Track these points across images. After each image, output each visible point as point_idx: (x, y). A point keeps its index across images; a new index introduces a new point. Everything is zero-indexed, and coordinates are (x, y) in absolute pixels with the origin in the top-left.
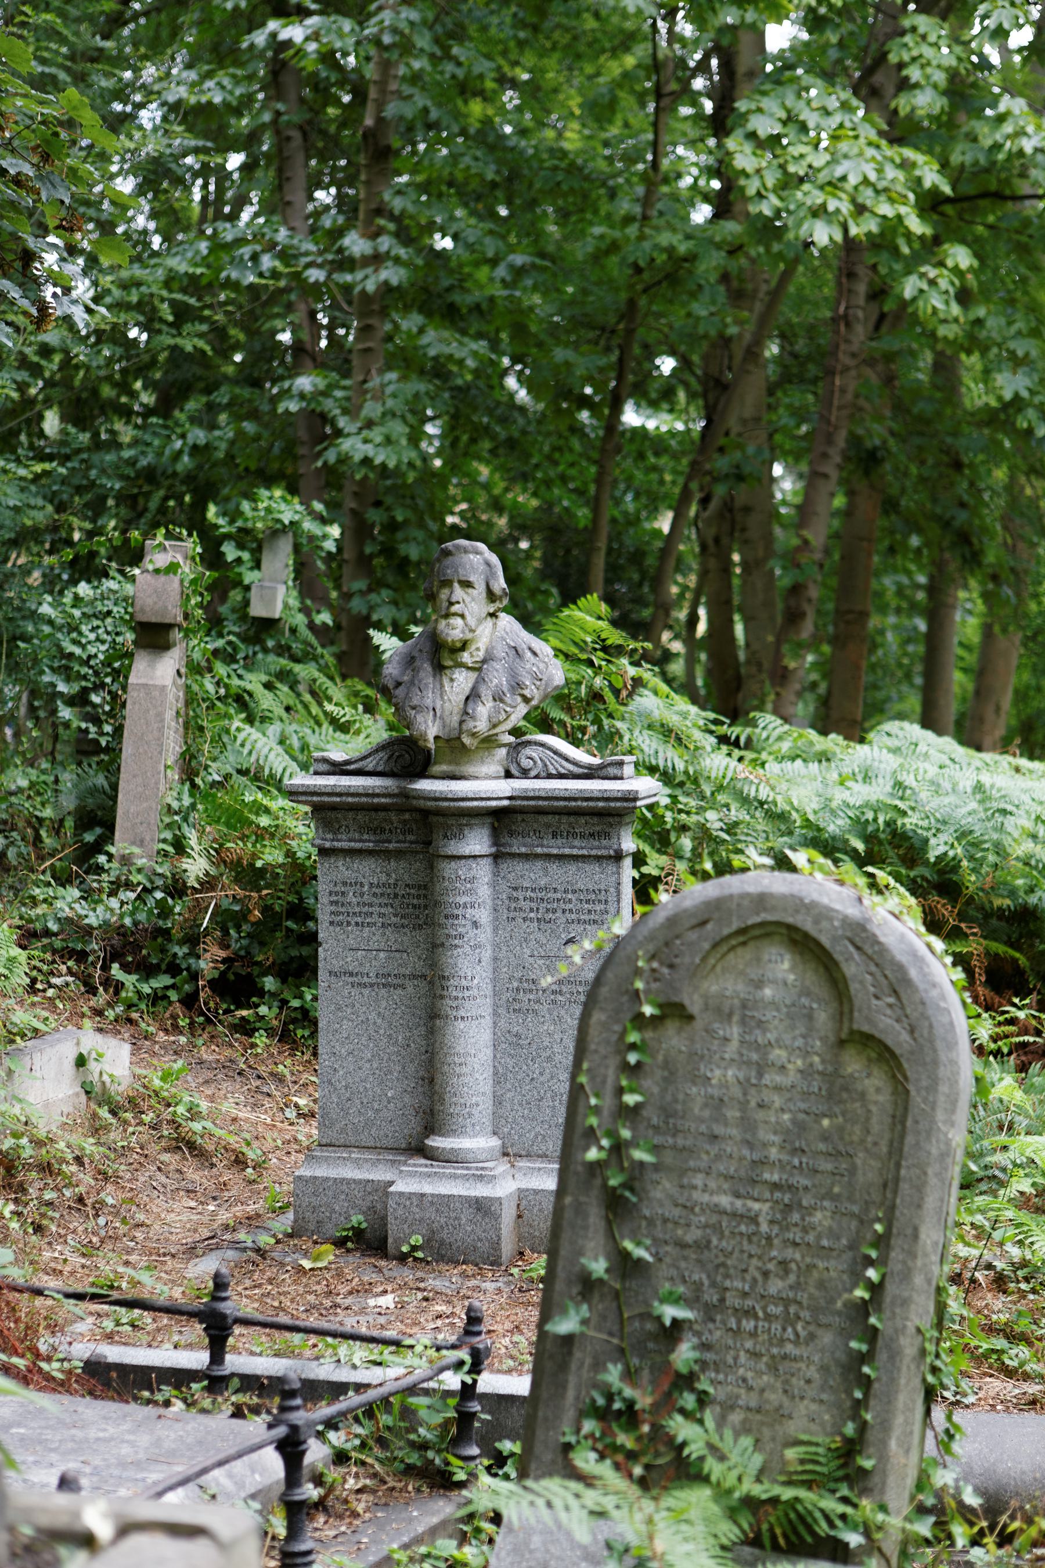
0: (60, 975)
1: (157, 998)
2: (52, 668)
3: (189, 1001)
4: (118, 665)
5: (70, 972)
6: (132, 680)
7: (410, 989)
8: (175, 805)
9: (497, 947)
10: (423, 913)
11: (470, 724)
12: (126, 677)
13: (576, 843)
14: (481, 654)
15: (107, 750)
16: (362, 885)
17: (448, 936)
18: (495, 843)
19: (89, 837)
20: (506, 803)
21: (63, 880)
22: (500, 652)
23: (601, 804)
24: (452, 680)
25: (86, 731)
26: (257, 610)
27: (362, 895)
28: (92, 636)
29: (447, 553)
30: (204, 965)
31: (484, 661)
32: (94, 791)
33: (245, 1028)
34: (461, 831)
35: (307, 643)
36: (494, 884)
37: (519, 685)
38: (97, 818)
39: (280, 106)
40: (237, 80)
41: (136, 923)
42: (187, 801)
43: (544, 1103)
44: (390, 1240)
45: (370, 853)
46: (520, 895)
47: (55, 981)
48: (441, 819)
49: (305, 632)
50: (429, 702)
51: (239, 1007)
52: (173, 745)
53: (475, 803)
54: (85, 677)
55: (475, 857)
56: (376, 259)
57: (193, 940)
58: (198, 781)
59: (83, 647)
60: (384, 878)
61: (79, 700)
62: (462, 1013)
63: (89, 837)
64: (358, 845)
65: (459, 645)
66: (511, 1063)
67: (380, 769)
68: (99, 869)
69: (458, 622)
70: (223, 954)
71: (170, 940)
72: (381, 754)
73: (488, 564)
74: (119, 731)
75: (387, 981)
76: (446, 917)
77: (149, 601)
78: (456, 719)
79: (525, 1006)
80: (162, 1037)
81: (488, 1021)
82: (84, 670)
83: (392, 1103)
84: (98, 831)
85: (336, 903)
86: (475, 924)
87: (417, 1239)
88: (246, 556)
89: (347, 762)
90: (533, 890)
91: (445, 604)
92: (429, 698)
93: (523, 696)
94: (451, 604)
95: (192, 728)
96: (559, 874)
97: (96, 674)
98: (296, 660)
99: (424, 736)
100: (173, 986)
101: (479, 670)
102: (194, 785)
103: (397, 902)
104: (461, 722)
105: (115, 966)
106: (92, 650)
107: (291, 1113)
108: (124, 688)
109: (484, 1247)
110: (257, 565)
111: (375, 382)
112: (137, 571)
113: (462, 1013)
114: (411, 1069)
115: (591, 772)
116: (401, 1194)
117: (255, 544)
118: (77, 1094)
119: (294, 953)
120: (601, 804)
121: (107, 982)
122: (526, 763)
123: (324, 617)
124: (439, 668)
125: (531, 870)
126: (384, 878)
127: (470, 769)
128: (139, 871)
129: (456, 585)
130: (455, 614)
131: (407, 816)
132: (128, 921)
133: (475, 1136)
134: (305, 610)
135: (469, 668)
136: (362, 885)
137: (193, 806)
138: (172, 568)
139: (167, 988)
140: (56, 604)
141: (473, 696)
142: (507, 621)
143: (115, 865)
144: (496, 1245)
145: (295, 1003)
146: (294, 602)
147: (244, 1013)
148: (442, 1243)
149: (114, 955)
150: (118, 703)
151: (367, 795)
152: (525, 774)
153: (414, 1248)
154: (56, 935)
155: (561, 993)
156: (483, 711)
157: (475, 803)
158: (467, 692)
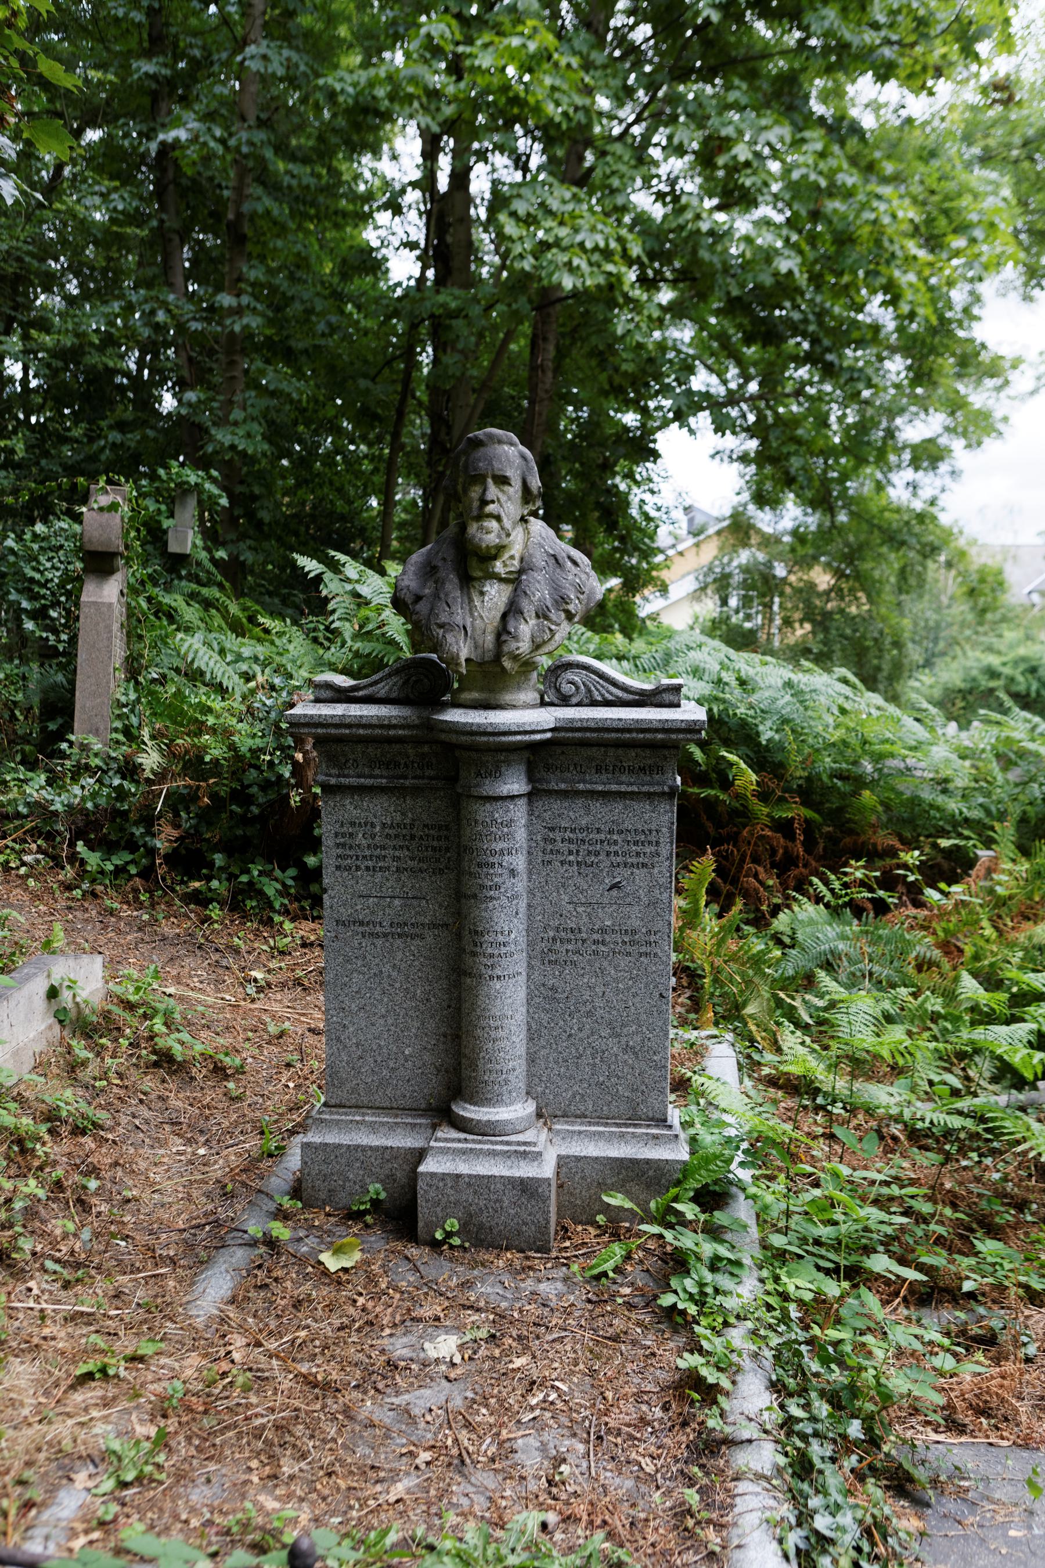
0: (30, 852)
1: (119, 871)
2: (17, 590)
3: (147, 873)
4: (71, 589)
5: (40, 850)
6: (84, 598)
7: (430, 939)
8: (123, 699)
9: (531, 892)
10: (450, 866)
12: (78, 597)
13: (624, 778)
15: (64, 654)
16: (373, 825)
17: (482, 887)
18: (531, 779)
19: (52, 726)
20: (549, 735)
21: (31, 765)
22: (539, 559)
23: (660, 736)
24: (482, 593)
25: (47, 639)
26: (173, 548)
27: (373, 836)
28: (48, 565)
29: (478, 443)
30: (160, 844)
31: (521, 572)
32: (55, 686)
33: (200, 900)
34: (498, 769)
35: (208, 572)
36: (529, 825)
38: (59, 708)
39: (164, 216)
40: (133, 195)
41: (96, 806)
42: (133, 696)
43: (584, 1061)
44: (420, 1224)
45: (382, 790)
46: (558, 835)
47: (28, 858)
48: (474, 755)
50: (458, 619)
51: (192, 878)
52: (119, 652)
53: (519, 738)
54: (44, 597)
55: (513, 797)
56: (238, 311)
57: (148, 820)
58: (141, 679)
59: (42, 573)
60: (398, 818)
61: (39, 615)
62: (498, 972)
63: (52, 726)
64: (368, 782)
66: (545, 1018)
67: (394, 695)
68: (63, 755)
69: (494, 524)
70: (175, 833)
71: (127, 820)
72: (394, 679)
73: (524, 457)
74: (73, 640)
75: (402, 931)
76: (480, 865)
77: (96, 534)
78: (490, 639)
79: (562, 957)
80: (126, 912)
81: (522, 979)
82: (43, 591)
83: (408, 1052)
84: (60, 721)
85: (343, 845)
86: (513, 873)
87: (452, 1224)
88: (163, 507)
90: (573, 831)
91: (476, 504)
94: (484, 503)
95: (132, 636)
96: (602, 813)
97: (53, 594)
98: (204, 585)
100: (132, 862)
102: (137, 683)
103: (414, 844)
105: (80, 843)
106: (49, 575)
107: (251, 990)
108: (77, 605)
109: (529, 1231)
110: (171, 515)
111: (238, 398)
112: (84, 509)
113: (498, 972)
114: (431, 1025)
115: (643, 699)
116: (433, 1175)
118: (50, 1027)
119: (239, 832)
120: (660, 736)
121: (73, 857)
122: (567, 689)
123: (221, 554)
124: (468, 581)
125: (569, 809)
126: (398, 818)
127: (508, 697)
128: (96, 755)
129: (490, 481)
131: (426, 749)
132: (89, 805)
133: (511, 1104)
134: (206, 548)
135: (501, 580)
136: (373, 825)
137: (138, 700)
138: (113, 507)
139: (127, 863)
140: (19, 538)
141: (512, 610)
142: (537, 526)
143: (75, 750)
144: (544, 1229)
145: (244, 878)
146: (199, 542)
147: (197, 884)
148: (481, 1226)
149: (79, 834)
150: (72, 618)
151: (381, 726)
152: (565, 701)
153: (449, 1235)
154: (26, 817)
155: (603, 943)
156: (525, 629)
157: (519, 738)
158: (502, 607)
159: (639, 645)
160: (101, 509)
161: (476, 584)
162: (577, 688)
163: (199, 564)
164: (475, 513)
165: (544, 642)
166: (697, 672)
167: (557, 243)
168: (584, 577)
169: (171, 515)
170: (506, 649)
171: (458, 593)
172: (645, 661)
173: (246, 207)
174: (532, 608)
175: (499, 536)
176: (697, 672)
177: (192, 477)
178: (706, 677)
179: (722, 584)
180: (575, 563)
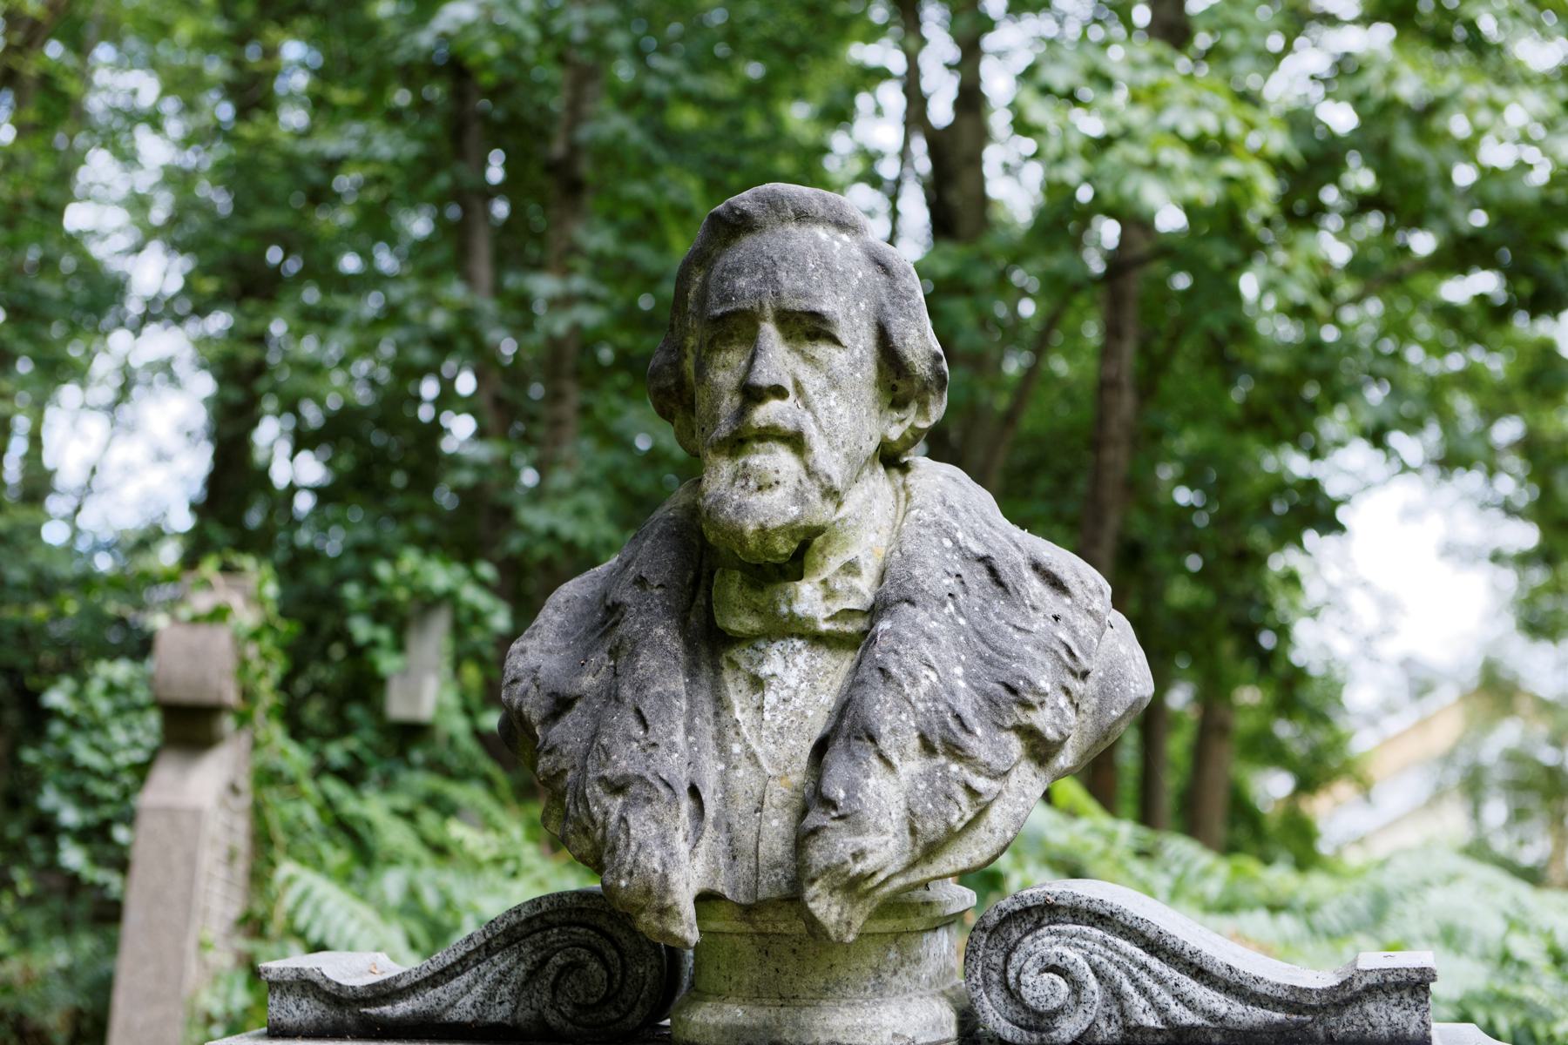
11: (837, 845)
14: (865, 587)
22: (935, 570)
24: (757, 684)
26: (398, 707)
31: (876, 611)
37: (1017, 694)
49: (467, 744)
50: (674, 766)
65: (783, 546)
69: (779, 461)
72: (501, 962)
78: (777, 827)
89: (385, 992)
91: (729, 403)
92: (678, 747)
93: (1029, 733)
94: (752, 394)
99: (656, 897)
101: (859, 642)
104: (803, 838)
110: (399, 646)
117: (399, 619)
124: (711, 646)
129: (769, 332)
130: (770, 434)
135: (819, 640)
138: (219, 614)
141: (847, 731)
156: (886, 797)
158: (818, 725)
159: (1316, 885)
160: (196, 620)
161: (740, 655)
162: (1076, 987)
163: (451, 741)
164: (724, 430)
165: (953, 835)
166: (1450, 937)
167: (1128, 134)
168: (1085, 625)
169: (399, 646)
170: (818, 856)
171: (679, 683)
172: (1330, 915)
173: (584, 133)
174: (908, 721)
175: (800, 498)
176: (1450, 937)
177: (440, 576)
178: (1474, 948)
179: (1474, 785)
180: (1056, 584)
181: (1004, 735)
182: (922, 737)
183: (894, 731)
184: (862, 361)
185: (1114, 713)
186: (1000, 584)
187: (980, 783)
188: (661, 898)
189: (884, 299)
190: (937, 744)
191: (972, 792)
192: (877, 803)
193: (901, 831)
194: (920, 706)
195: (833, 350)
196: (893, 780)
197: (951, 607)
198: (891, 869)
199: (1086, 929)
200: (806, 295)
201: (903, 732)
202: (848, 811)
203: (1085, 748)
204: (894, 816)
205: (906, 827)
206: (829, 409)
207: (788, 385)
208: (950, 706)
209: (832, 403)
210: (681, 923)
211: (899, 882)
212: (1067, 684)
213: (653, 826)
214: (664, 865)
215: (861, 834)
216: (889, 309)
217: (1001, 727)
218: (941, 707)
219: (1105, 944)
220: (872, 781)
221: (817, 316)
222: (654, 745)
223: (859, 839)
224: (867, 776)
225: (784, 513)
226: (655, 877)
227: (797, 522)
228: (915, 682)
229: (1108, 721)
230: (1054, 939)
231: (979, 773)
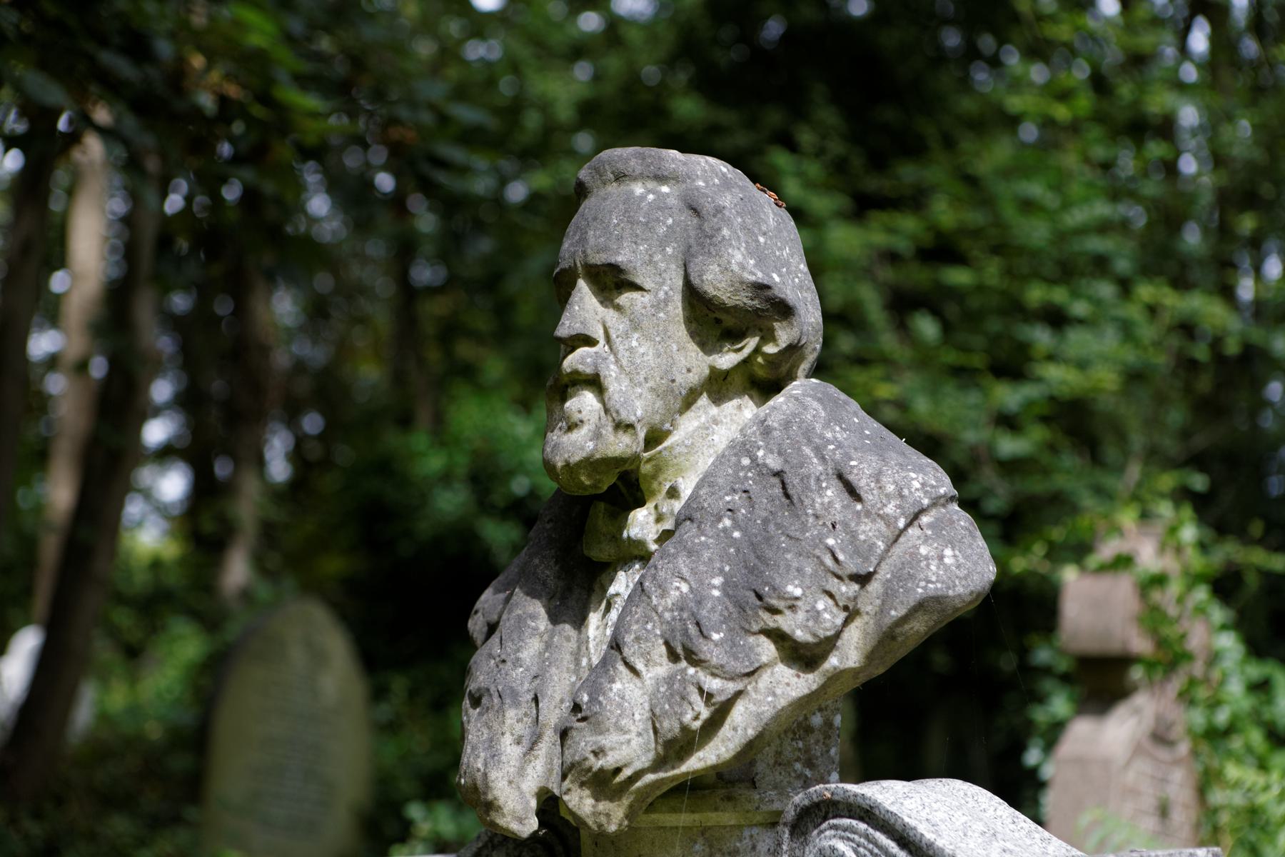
181: (751, 639)
182: (667, 643)
183: (638, 639)
184: (666, 301)
185: (893, 613)
186: (787, 496)
187: (713, 684)
188: (485, 794)
189: (692, 241)
190: (679, 650)
191: (708, 697)
192: (620, 706)
193: (646, 730)
194: (667, 615)
195: (635, 295)
196: (639, 684)
197: (727, 522)
198: (638, 765)
199: (854, 822)
200: (605, 249)
201: (647, 640)
202: (588, 713)
203: (869, 648)
204: (637, 717)
205: (650, 726)
206: (631, 350)
207: (599, 334)
208: (693, 614)
209: (634, 344)
210: (504, 815)
211: (650, 777)
212: (828, 587)
213: (486, 731)
214: (486, 765)
215: (601, 734)
216: (695, 249)
217: (749, 632)
218: (685, 615)
219: (867, 837)
220: (617, 686)
221: (615, 269)
222: (504, 661)
223: (599, 738)
224: (612, 681)
225: (582, 448)
226: (479, 776)
227: (592, 455)
228: (664, 594)
229: (888, 621)
230: (833, 832)
231: (714, 675)
